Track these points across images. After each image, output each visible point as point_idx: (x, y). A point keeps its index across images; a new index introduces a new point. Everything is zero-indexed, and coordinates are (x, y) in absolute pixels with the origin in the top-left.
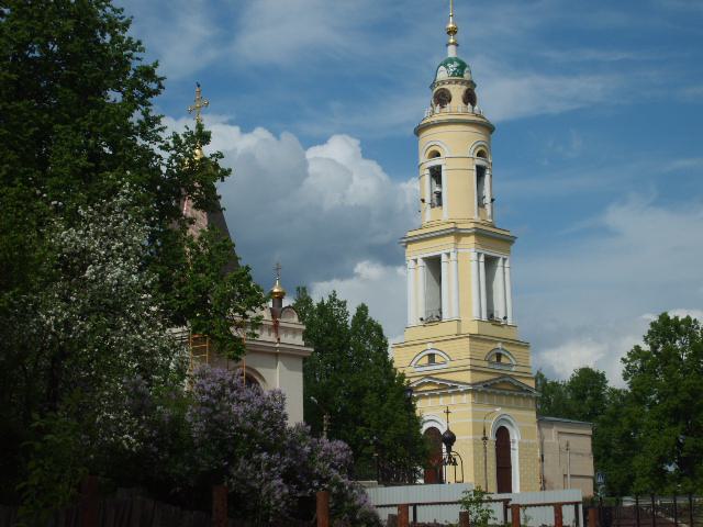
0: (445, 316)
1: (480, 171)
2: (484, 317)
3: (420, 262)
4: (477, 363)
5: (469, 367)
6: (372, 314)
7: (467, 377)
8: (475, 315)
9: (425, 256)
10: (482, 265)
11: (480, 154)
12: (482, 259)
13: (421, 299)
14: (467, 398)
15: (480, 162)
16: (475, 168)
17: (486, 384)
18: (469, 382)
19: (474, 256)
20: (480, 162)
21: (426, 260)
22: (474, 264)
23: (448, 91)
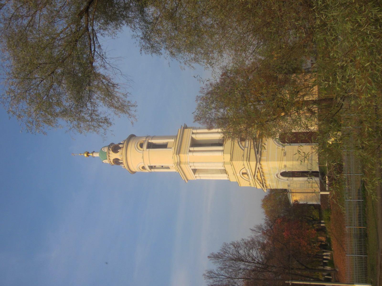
0: (223, 168)
1: (151, 146)
2: (221, 148)
3: (196, 175)
4: (245, 156)
5: (248, 162)
6: (217, 250)
7: (253, 164)
8: (220, 154)
9: (193, 174)
10: (196, 149)
11: (141, 146)
12: (192, 149)
13: (211, 178)
14: (263, 163)
15: (145, 146)
16: (148, 150)
17: (257, 152)
18: (255, 162)
19: (191, 154)
20: (145, 146)
21: (194, 173)
22: (195, 154)
23: (114, 160)
